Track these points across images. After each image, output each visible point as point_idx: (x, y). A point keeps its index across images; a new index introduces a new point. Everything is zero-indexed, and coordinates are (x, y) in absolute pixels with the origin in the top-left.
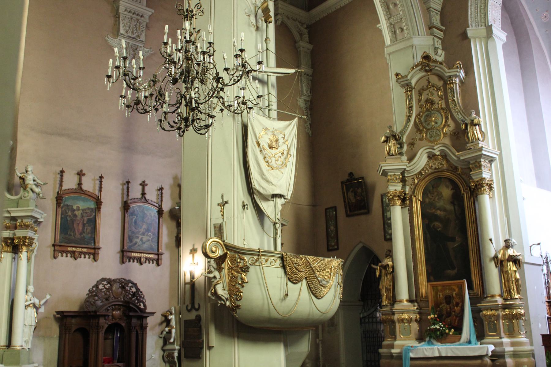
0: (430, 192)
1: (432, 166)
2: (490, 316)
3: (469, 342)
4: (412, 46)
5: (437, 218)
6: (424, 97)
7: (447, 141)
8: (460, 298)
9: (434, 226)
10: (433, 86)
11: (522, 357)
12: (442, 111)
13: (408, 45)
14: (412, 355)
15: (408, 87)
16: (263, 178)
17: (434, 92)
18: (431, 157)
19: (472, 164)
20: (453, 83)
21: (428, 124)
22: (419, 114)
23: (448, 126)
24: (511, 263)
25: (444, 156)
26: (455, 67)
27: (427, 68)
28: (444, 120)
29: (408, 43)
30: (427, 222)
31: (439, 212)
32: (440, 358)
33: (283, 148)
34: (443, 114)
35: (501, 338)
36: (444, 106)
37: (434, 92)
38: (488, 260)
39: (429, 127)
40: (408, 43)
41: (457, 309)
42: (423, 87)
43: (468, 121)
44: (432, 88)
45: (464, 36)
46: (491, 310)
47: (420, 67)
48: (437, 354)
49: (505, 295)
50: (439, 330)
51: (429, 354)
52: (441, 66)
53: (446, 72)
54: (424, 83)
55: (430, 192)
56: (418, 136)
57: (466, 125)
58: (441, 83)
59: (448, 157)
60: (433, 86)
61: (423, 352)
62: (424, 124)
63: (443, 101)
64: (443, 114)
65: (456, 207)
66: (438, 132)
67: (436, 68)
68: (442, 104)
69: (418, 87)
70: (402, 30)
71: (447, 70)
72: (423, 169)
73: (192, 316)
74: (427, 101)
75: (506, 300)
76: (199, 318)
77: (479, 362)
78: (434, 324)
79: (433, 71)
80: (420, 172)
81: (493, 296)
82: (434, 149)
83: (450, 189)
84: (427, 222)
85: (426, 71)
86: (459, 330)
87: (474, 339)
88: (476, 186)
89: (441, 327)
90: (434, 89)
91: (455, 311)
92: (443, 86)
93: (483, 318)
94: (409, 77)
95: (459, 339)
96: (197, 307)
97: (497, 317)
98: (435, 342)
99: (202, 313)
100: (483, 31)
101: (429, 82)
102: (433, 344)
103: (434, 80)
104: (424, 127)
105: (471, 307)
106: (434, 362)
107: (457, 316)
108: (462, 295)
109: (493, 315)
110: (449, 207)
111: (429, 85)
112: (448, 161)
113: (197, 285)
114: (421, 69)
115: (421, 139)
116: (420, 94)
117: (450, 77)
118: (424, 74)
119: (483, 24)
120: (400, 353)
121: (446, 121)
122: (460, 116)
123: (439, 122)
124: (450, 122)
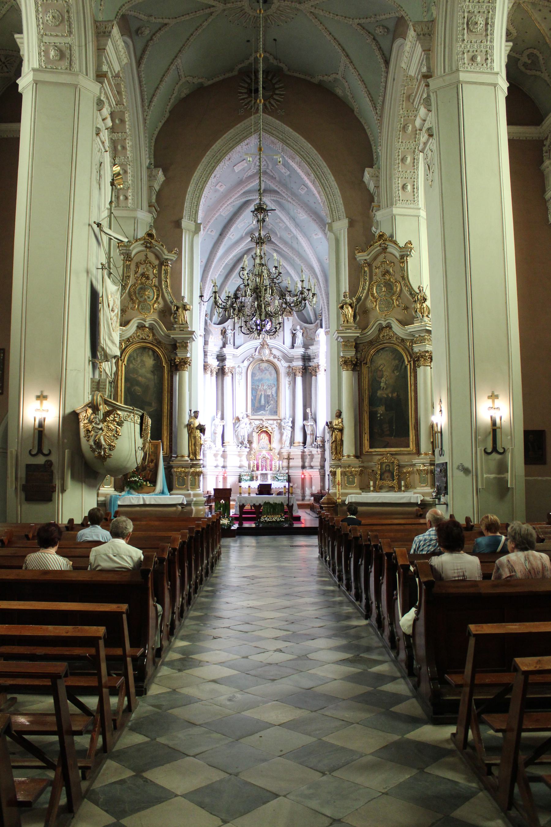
0: (134, 359)
1: (139, 336)
2: (180, 473)
3: (163, 493)
4: (135, 218)
5: (138, 384)
6: (140, 271)
7: (156, 317)
8: (154, 456)
9: (135, 389)
10: (150, 263)
11: (200, 506)
12: (154, 288)
13: (132, 216)
14: (119, 503)
15: (127, 257)
16: (109, 339)
17: (150, 268)
18: (141, 327)
19: (179, 343)
20: (168, 266)
21: (141, 297)
22: (135, 285)
23: (159, 303)
24: (199, 431)
25: (152, 328)
26: (173, 252)
27: (148, 245)
28: (155, 297)
29: (132, 214)
30: (129, 385)
31: (140, 379)
32: (145, 505)
33: (116, 312)
34: (155, 291)
35: (188, 490)
36: (157, 284)
37: (150, 268)
38: (183, 426)
39: (142, 300)
40: (132, 214)
41: (152, 465)
42: (141, 260)
43: (179, 305)
44: (149, 265)
45: (178, 224)
46: (183, 468)
47: (142, 242)
48: (141, 502)
49: (191, 456)
50: (138, 482)
51: (135, 502)
52: (161, 247)
53: (164, 254)
54: (142, 257)
55: (134, 359)
56: (131, 305)
57: (178, 308)
58: (156, 262)
59: (154, 331)
60: (150, 263)
61: (130, 500)
62: (137, 295)
63: (157, 279)
64: (155, 291)
65: (156, 377)
66: (149, 306)
67: (157, 248)
68: (155, 281)
69: (136, 260)
70: (126, 198)
71: (166, 252)
72: (131, 337)
73: (41, 460)
74: (143, 275)
75: (192, 460)
76: (49, 464)
77: (174, 509)
78: (133, 477)
79: (152, 249)
80: (128, 339)
81: (183, 456)
82: (145, 322)
83: (152, 360)
84: (129, 385)
85: (146, 247)
86: (154, 482)
87: (166, 490)
88: (180, 362)
89: (140, 479)
90: (150, 266)
91: (149, 467)
92: (158, 265)
93: (174, 474)
94: (131, 248)
95: (154, 490)
96: (46, 451)
97: (187, 474)
98: (134, 492)
99: (54, 458)
100: (192, 226)
101: (147, 258)
102: (131, 494)
103: (152, 257)
104: (137, 298)
105: (526, 475)
106: (138, 509)
107: (150, 471)
108: (157, 453)
109: (184, 472)
110: (150, 376)
111: (146, 261)
112: (154, 335)
113: (46, 431)
114: (143, 244)
115: (133, 309)
116: (137, 266)
117: (167, 259)
118: (143, 248)
119: (193, 219)
120: (105, 501)
121: (157, 299)
122: (170, 298)
123: (151, 298)
124: (160, 299)
